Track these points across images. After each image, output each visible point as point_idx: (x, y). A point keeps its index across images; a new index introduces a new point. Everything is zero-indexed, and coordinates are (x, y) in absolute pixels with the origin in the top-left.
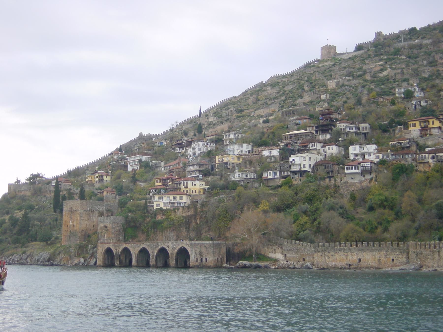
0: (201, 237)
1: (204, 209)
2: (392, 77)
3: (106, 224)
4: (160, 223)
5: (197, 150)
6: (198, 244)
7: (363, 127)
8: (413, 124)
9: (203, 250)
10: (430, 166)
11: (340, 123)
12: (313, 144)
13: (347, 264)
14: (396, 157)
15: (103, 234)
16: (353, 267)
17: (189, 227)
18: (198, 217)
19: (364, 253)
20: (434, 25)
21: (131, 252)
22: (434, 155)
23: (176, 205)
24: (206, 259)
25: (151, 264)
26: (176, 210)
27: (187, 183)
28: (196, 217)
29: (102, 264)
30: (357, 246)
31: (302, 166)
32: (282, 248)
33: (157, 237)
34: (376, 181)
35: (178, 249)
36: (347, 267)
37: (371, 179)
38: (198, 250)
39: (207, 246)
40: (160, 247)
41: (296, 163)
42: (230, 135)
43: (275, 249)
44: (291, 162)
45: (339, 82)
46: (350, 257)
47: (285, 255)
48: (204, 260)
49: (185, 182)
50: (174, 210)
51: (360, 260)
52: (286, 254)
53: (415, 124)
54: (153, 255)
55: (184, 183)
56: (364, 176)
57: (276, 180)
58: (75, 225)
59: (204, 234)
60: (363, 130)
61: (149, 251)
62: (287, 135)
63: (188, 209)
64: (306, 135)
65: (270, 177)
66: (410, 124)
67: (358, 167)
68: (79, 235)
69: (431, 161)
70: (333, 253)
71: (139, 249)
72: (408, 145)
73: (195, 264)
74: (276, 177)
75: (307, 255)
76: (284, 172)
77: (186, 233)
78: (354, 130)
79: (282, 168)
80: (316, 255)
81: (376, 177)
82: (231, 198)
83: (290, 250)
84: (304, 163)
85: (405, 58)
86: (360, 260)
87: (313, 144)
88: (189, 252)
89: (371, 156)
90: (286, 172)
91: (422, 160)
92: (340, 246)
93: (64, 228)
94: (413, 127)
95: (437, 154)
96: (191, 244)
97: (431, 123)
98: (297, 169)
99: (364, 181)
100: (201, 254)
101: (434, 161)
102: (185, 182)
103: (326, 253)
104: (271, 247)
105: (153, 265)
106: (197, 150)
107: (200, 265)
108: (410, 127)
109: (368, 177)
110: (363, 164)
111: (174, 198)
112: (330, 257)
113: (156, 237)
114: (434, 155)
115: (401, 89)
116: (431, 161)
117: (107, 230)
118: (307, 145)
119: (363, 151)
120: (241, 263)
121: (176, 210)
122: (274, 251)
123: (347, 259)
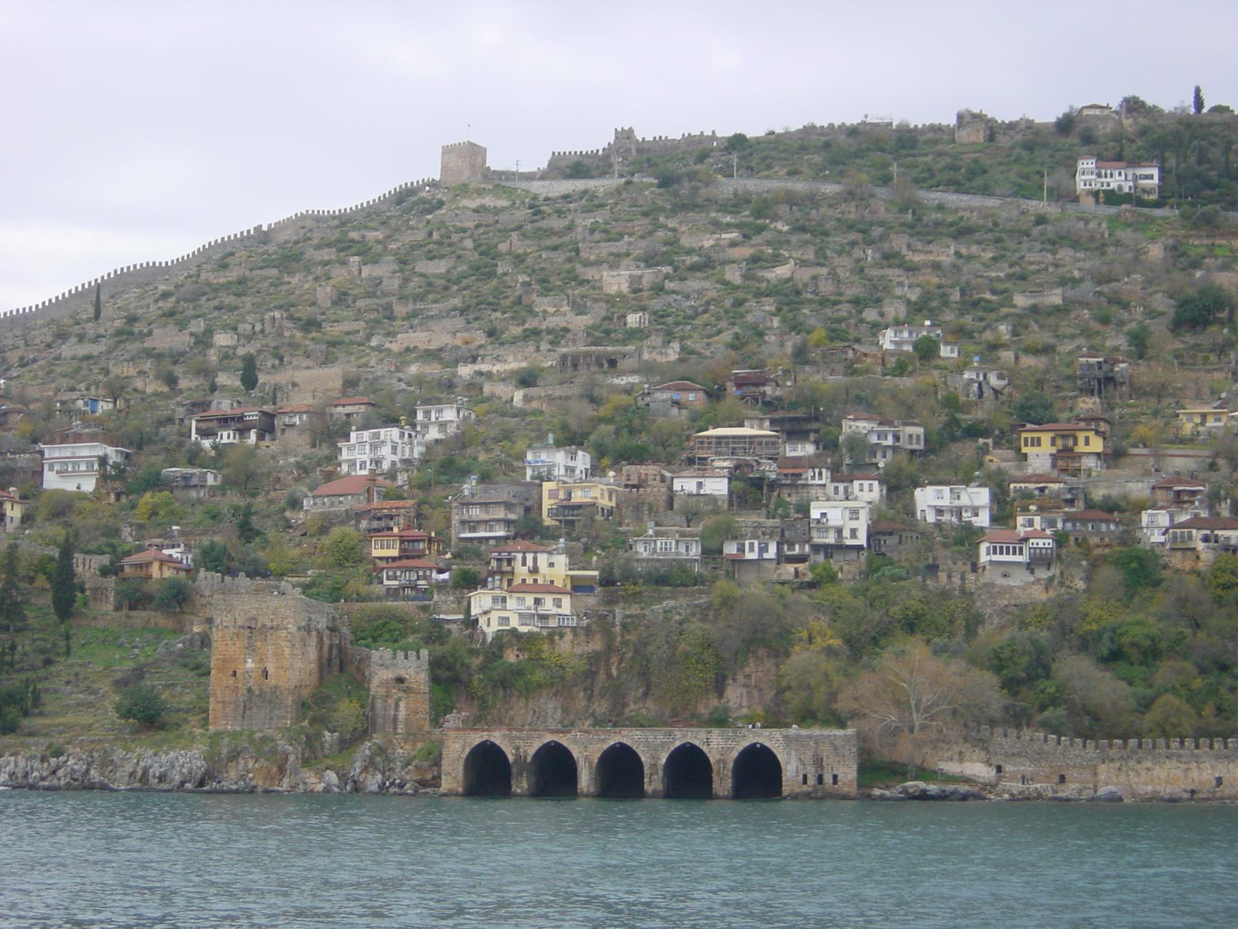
0: (623, 713)
1: (627, 637)
2: (805, 285)
3: (402, 673)
4: (518, 672)
5: (386, 451)
6: (810, 737)
7: (911, 436)
8: (1032, 439)
9: (825, 751)
10: (1198, 557)
11: (854, 420)
12: (817, 471)
13: (1185, 791)
14: (1074, 525)
15: (391, 702)
16: (1201, 796)
17: (592, 684)
18: (614, 660)
19: (1231, 765)
20: (787, 134)
21: (575, 754)
22: (1208, 532)
23: (553, 623)
24: (835, 777)
25: (648, 788)
26: (557, 638)
27: (535, 560)
28: (608, 660)
29: (461, 790)
30: (1211, 747)
31: (846, 533)
32: (985, 749)
33: (512, 713)
34: (1061, 584)
35: (740, 748)
36: (1186, 795)
37: (1051, 579)
38: (809, 754)
39: (839, 743)
40: (678, 744)
41: (831, 523)
42: (441, 411)
43: (961, 753)
44: (818, 521)
45: (641, 277)
46: (1195, 774)
47: (999, 769)
48: (828, 779)
49: (530, 557)
50: (550, 637)
51: (1219, 781)
52: (1001, 763)
53: (1039, 439)
54: (654, 766)
55: (524, 559)
56: (1032, 572)
57: (767, 565)
58: (271, 671)
59: (632, 706)
60: (911, 443)
61: (640, 755)
62: (708, 437)
63: (587, 635)
64: (767, 443)
65: (749, 556)
66: (1026, 439)
67: (1021, 549)
68: (290, 701)
69: (1201, 546)
70: (1149, 765)
71: (605, 747)
72: (1069, 496)
73: (798, 790)
74: (766, 556)
75: (1074, 766)
76: (791, 545)
77: (584, 703)
78: (890, 441)
79: (787, 533)
80: (1102, 768)
81: (1062, 573)
82: (697, 611)
83: (1013, 755)
84: (854, 524)
85: (786, 228)
86: (1219, 781)
87: (817, 471)
88: (780, 757)
89: (977, 515)
90: (797, 547)
91: (1183, 542)
92: (1168, 747)
93: (218, 681)
94: (1033, 445)
95: (1216, 532)
96: (786, 737)
97: (1081, 441)
98: (831, 539)
99: (1033, 583)
100: (819, 762)
101: (1208, 548)
102: (530, 557)
103: (1132, 763)
104: (946, 747)
105: (655, 791)
106: (386, 451)
107: (816, 791)
108: (1026, 445)
109: (1043, 574)
110: (1035, 541)
111: (537, 602)
112: (1143, 773)
113: (507, 711)
114: (1208, 532)
115: (901, 332)
116: (1201, 546)
117: (408, 691)
118: (800, 475)
119: (956, 503)
120: (912, 787)
121: (557, 638)
122: (956, 757)
123: (1186, 777)
